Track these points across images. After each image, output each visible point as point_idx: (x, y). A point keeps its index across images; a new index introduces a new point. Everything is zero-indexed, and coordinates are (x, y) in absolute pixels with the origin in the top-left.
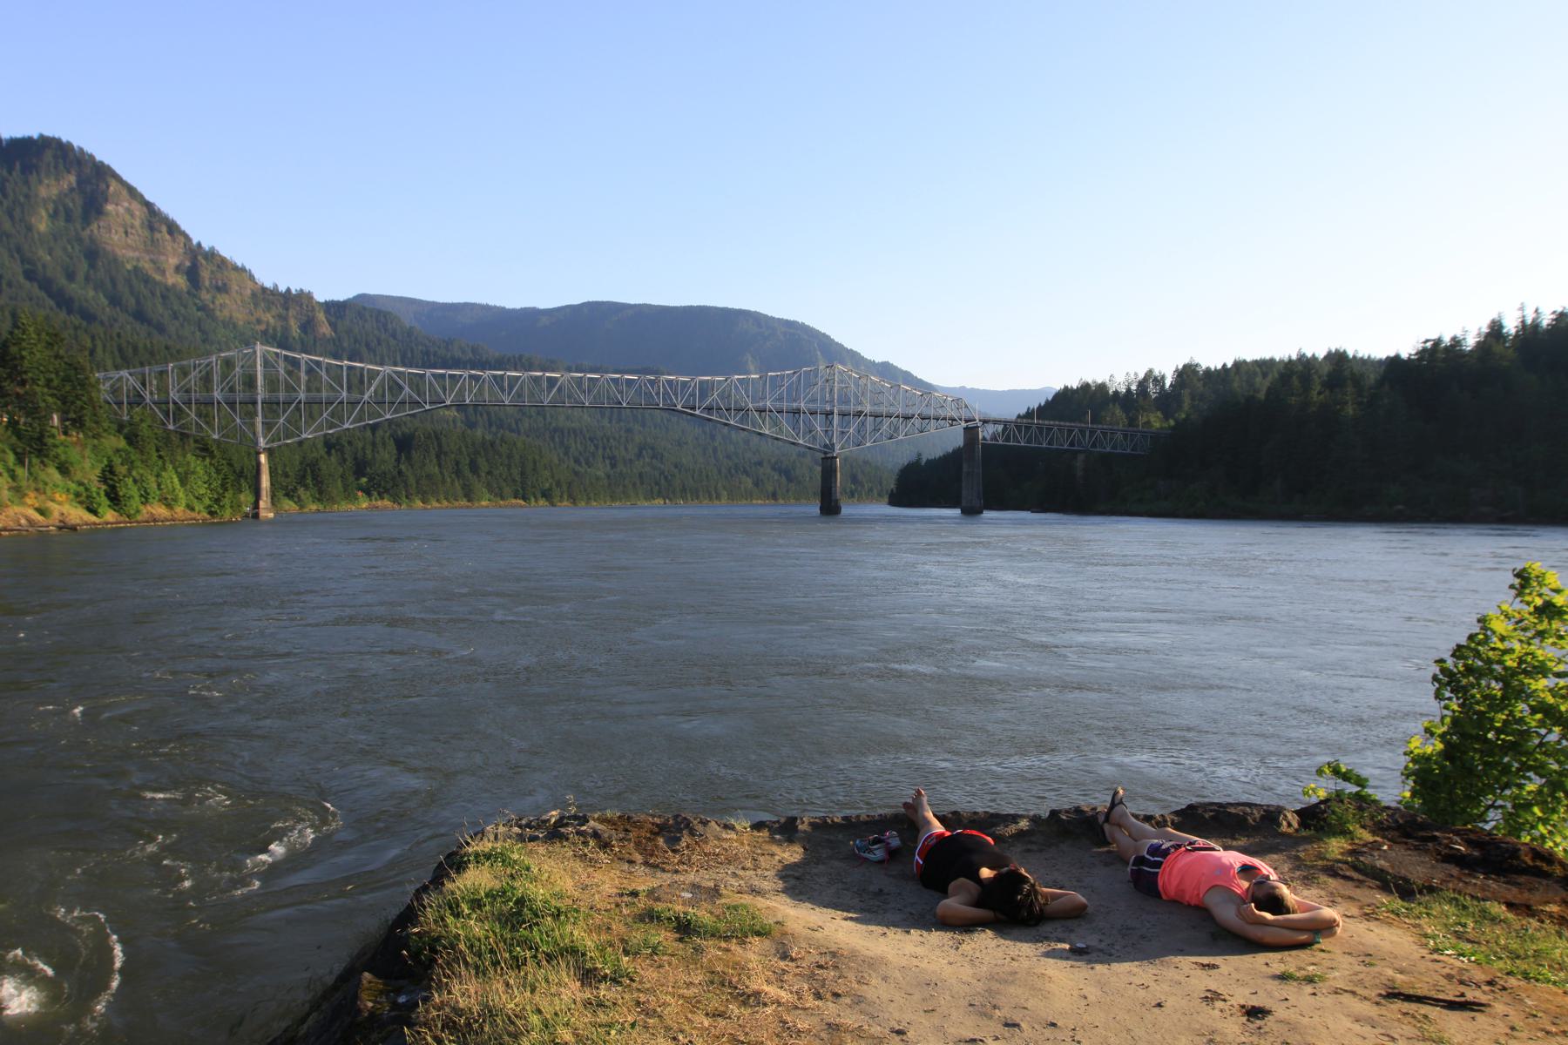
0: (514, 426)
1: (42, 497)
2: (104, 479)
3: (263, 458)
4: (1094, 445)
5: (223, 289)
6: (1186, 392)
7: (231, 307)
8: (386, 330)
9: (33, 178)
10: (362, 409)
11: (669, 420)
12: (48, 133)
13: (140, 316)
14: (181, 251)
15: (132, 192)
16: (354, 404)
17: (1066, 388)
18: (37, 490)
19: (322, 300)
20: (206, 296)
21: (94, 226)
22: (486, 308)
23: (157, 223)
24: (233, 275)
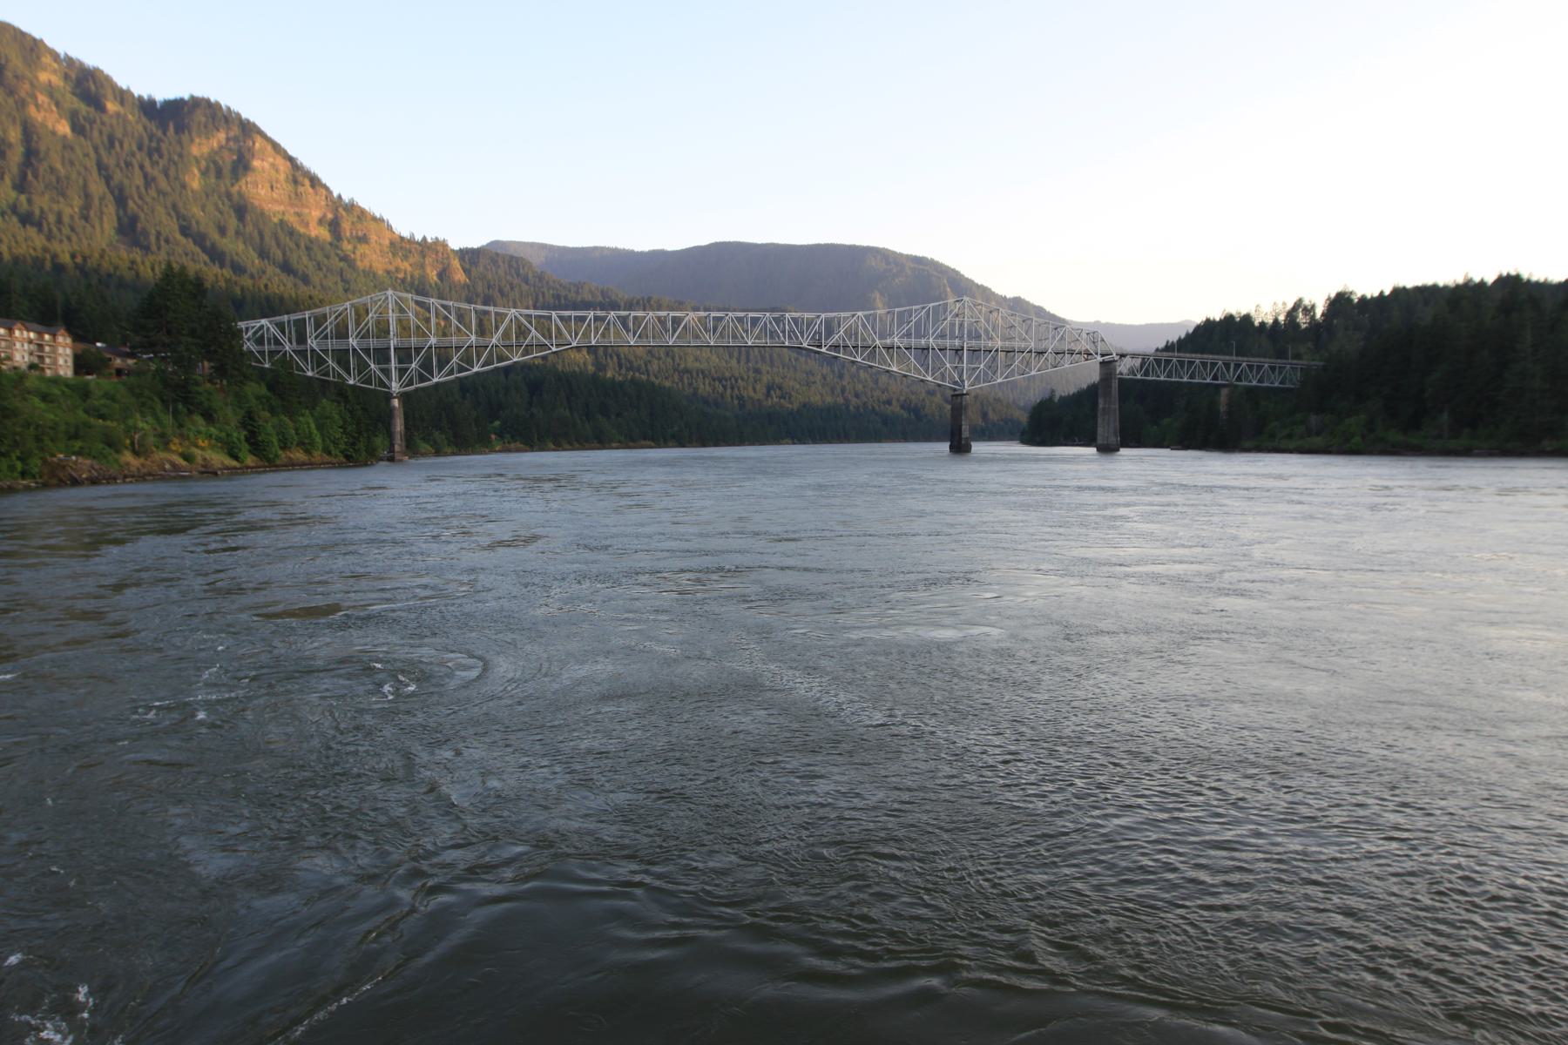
3: (396, 403)
5: (363, 239)
9: (185, 137)
13: (287, 268)
15: (276, 147)
16: (480, 349)
20: (347, 247)
23: (301, 177)
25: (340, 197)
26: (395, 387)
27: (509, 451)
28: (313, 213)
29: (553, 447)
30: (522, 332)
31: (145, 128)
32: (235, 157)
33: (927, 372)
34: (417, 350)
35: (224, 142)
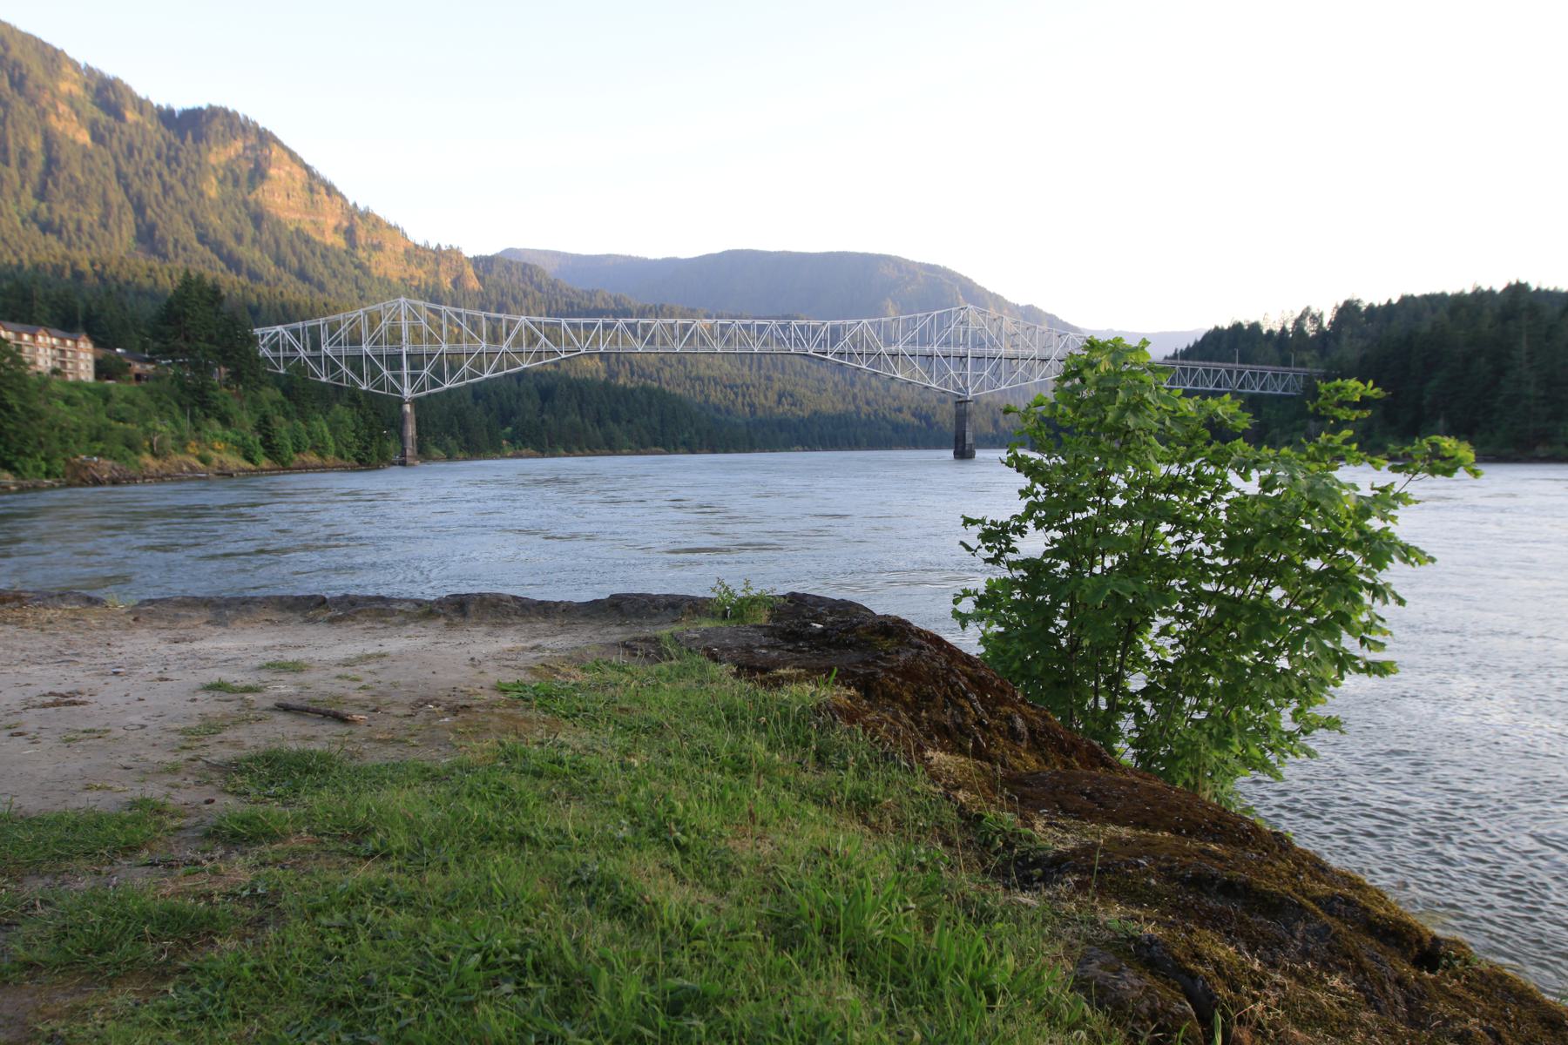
0: (655, 376)
1: (203, 446)
2: (259, 429)
3: (408, 408)
4: (1242, 386)
5: (378, 247)
6: (1346, 330)
7: (387, 266)
8: (532, 283)
9: (203, 147)
10: (501, 360)
11: (808, 367)
12: (216, 103)
13: (302, 276)
14: (339, 211)
15: (293, 156)
17: (1216, 328)
18: (199, 439)
19: (470, 256)
20: (362, 254)
21: (259, 191)
22: (629, 260)
23: (316, 186)
24: (388, 233)
25: (355, 205)
26: (407, 393)
27: (521, 456)
28: (329, 221)
30: (533, 340)
31: (163, 137)
32: (252, 166)
33: (931, 378)
34: (430, 356)
35: (241, 151)
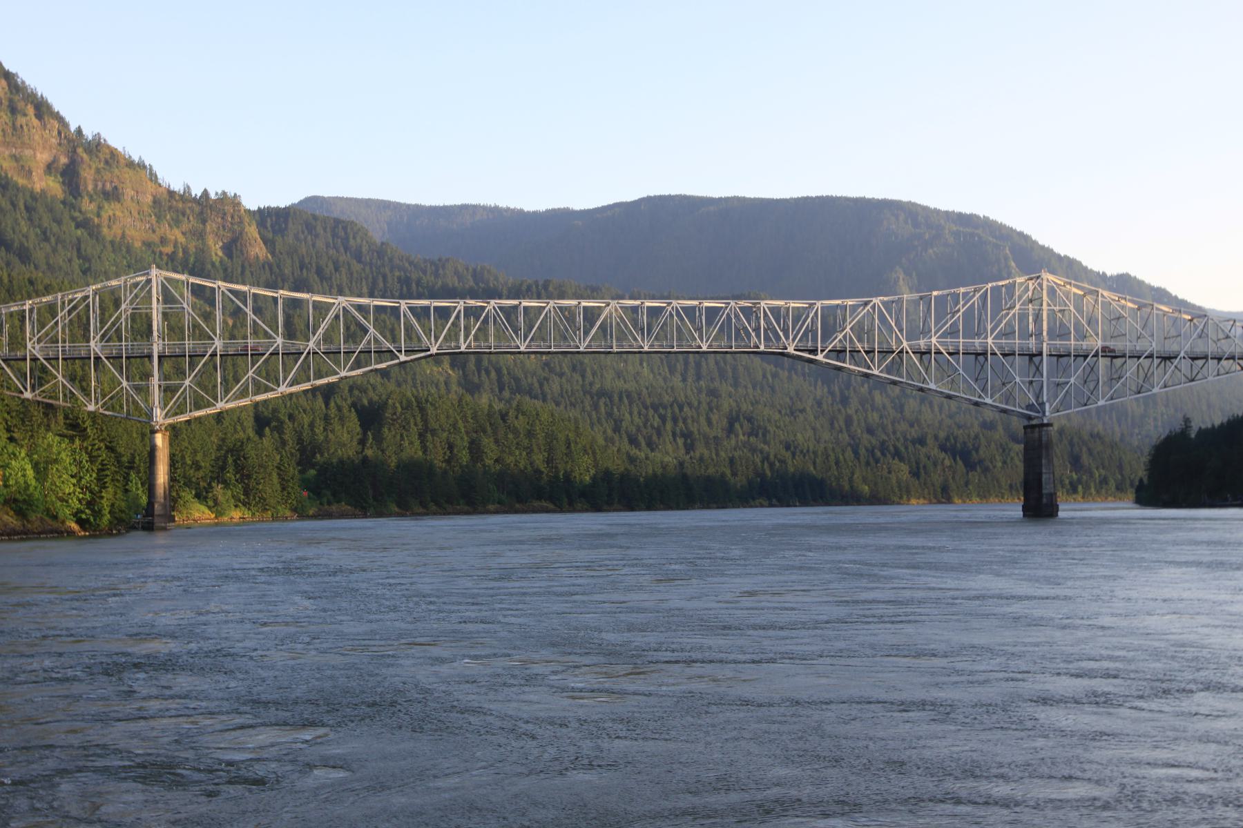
5: (113, 195)
20: (88, 206)
22: (495, 213)
25: (79, 131)
27: (330, 516)
29: (397, 510)
